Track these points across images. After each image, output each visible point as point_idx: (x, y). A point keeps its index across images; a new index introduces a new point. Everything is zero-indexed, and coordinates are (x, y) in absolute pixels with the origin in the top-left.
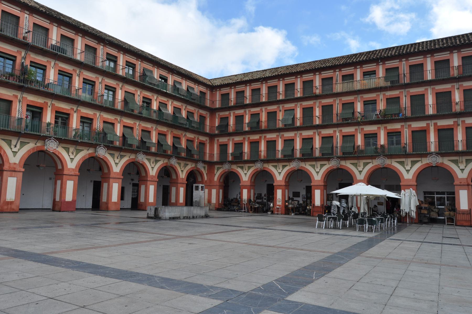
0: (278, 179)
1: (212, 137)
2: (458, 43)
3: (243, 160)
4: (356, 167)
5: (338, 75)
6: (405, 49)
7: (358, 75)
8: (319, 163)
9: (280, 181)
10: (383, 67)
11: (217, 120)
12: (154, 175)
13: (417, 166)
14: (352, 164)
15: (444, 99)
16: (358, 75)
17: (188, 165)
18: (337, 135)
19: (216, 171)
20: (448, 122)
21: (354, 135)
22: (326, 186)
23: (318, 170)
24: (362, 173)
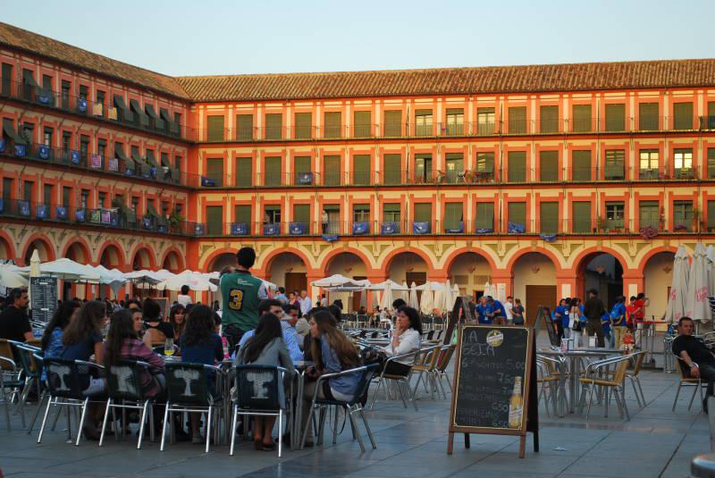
0: (313, 267)
1: (192, 191)
2: (684, 82)
3: (252, 234)
4: (496, 252)
5: (408, 107)
6: (505, 82)
7: (471, 108)
8: (504, 243)
9: (317, 270)
10: (474, 105)
11: (201, 163)
13: (514, 251)
14: (429, 246)
15: (548, 159)
16: (471, 108)
17: (134, 240)
18: (406, 198)
19: (200, 252)
20: (247, 151)
21: (557, 202)
22: (491, 278)
23: (377, 254)
24: (505, 259)
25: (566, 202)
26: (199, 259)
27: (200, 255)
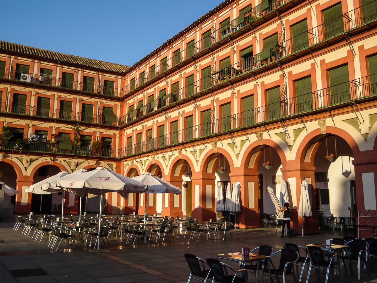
12: (294, 158)
25: (357, 61)
26: (124, 173)
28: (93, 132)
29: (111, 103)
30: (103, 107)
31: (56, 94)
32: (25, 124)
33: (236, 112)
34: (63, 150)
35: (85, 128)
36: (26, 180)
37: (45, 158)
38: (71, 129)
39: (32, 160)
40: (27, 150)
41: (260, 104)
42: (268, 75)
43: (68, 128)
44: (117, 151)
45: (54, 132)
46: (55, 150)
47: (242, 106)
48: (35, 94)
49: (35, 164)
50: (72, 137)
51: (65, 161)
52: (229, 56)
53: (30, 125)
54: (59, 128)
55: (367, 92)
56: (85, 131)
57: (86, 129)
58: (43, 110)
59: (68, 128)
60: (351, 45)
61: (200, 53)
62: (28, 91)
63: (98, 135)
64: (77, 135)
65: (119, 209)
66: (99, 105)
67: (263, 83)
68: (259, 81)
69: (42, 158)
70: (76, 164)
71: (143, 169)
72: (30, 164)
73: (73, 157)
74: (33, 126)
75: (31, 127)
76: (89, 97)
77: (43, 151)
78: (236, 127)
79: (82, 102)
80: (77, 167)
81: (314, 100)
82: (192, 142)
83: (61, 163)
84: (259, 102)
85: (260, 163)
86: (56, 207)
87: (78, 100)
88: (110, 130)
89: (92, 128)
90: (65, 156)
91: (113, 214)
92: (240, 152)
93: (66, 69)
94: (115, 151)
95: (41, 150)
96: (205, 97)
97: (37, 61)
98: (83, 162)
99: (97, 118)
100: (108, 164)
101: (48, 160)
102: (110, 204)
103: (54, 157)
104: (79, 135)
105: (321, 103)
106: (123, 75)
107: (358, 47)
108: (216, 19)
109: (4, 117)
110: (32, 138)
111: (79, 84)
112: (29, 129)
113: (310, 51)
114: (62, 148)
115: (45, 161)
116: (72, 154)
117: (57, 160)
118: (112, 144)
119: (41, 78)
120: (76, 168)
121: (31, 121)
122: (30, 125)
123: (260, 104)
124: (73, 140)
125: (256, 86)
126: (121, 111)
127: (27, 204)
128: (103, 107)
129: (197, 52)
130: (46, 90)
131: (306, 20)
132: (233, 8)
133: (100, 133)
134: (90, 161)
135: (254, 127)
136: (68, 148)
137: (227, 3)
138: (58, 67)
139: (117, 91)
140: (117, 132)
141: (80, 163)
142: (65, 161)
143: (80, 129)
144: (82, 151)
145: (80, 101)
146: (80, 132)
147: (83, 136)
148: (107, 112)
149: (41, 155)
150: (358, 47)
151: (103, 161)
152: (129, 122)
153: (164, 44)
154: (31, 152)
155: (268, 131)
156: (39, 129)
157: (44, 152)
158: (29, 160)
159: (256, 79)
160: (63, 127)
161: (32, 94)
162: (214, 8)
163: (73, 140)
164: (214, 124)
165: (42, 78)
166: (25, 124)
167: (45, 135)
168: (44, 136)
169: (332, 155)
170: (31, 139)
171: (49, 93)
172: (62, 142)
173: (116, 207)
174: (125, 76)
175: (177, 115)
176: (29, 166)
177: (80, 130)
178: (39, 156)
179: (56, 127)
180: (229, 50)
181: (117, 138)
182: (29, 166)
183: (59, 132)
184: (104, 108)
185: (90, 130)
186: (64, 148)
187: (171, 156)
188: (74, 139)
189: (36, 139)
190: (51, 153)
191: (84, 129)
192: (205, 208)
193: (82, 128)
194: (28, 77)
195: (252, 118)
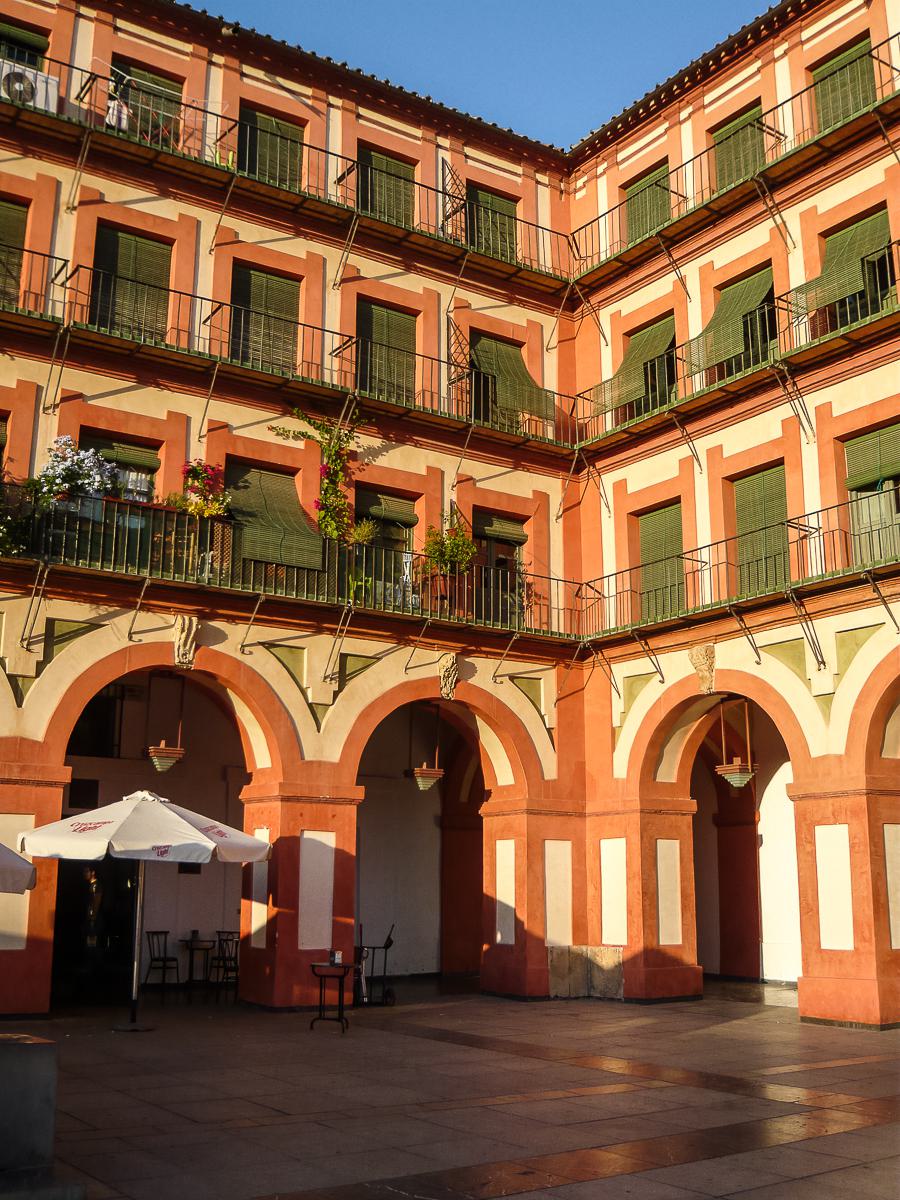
19: (618, 705)
26: (613, 733)
27: (616, 723)
28: (424, 472)
29: (513, 316)
30: (473, 330)
31: (209, 220)
32: (14, 385)
33: (610, 566)
34: (267, 563)
35: (377, 442)
36: (23, 769)
37: (145, 620)
38: (300, 445)
39: (59, 630)
40: (33, 550)
41: (704, 536)
42: (874, 364)
43: (284, 434)
44: (558, 596)
45: (198, 453)
46: (209, 567)
47: (633, 541)
48: (81, 203)
49: (79, 660)
50: (305, 489)
51: (269, 645)
52: (671, 312)
53: (50, 396)
54: (226, 426)
55: (864, 550)
56: (382, 461)
57: (386, 449)
58: (125, 306)
59: (284, 434)
60: (690, 443)
61: (616, 259)
62: (39, 176)
63: (450, 495)
64: (333, 482)
65: (589, 965)
66: (448, 319)
67: (715, 452)
68: (703, 444)
69: (124, 621)
70: (337, 669)
71: (826, 699)
72: (48, 657)
73: (320, 618)
74: (63, 400)
75: (56, 406)
76: (394, 263)
77: (142, 565)
78: (708, 602)
79: (355, 288)
80: (341, 689)
81: (793, 548)
82: (802, 595)
83: (247, 660)
84: (703, 524)
85: (704, 762)
86: (170, 954)
87: (333, 273)
88: (515, 468)
89: (417, 444)
90: (276, 611)
91: (556, 997)
92: (835, 689)
93: (260, 86)
94: (549, 599)
95: (130, 561)
96: (863, 358)
97: (92, 13)
98: (377, 658)
99: (444, 393)
100: (512, 678)
101: (167, 633)
102: (537, 932)
103: (203, 617)
104: (348, 485)
105: (708, 592)
106: (562, 165)
107: (707, 450)
108: (604, 172)
109: (194, 393)
110: (71, 475)
111: (340, 180)
112: (42, 417)
113: (675, 419)
114: (259, 553)
115: (147, 638)
116: (323, 600)
117: (221, 637)
118: (525, 554)
119: (120, 112)
120: (336, 694)
121: (57, 368)
122: (50, 396)
123: (704, 536)
124: (316, 515)
125: (687, 464)
126: (582, 364)
127: (21, 946)
128: (473, 330)
129: (596, 263)
130: (146, 186)
131: (671, 317)
132: (597, 177)
133: (464, 481)
134: (423, 655)
135: (689, 623)
136: (295, 558)
137: (620, 126)
138: (213, 69)
139: (534, 251)
140: (552, 486)
141: (360, 664)
142: (269, 645)
143: (352, 446)
144: (380, 584)
145: (344, 281)
146: (351, 464)
147: (368, 492)
148: (488, 363)
149: (122, 594)
150: (614, 484)
151: (488, 654)
152: (626, 425)
153: (637, 106)
154: (60, 566)
155: (653, 658)
156: (102, 425)
157: (145, 573)
158: (40, 629)
159: (688, 438)
160: (256, 426)
161: (64, 198)
162: (658, 86)
163: (316, 515)
164: (601, 597)
165: (125, 110)
166: (14, 385)
167: (139, 468)
168: (133, 476)
169: (737, 761)
170: (64, 480)
171: (168, 209)
172: (251, 515)
173: (569, 951)
174: (569, 175)
175: (777, 433)
176: (40, 667)
177: (353, 455)
178: (106, 602)
179: (211, 421)
180: (669, 288)
181: (553, 518)
182: (40, 667)
183: (229, 457)
184: (476, 334)
185: (407, 461)
186: (271, 554)
187: (636, 681)
188: (321, 506)
189: (98, 478)
190: (192, 581)
191: (374, 453)
192: (654, 944)
193: (364, 441)
194: (40, 87)
195: (680, 586)
